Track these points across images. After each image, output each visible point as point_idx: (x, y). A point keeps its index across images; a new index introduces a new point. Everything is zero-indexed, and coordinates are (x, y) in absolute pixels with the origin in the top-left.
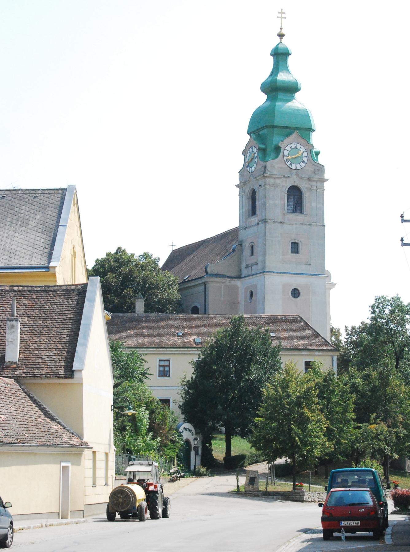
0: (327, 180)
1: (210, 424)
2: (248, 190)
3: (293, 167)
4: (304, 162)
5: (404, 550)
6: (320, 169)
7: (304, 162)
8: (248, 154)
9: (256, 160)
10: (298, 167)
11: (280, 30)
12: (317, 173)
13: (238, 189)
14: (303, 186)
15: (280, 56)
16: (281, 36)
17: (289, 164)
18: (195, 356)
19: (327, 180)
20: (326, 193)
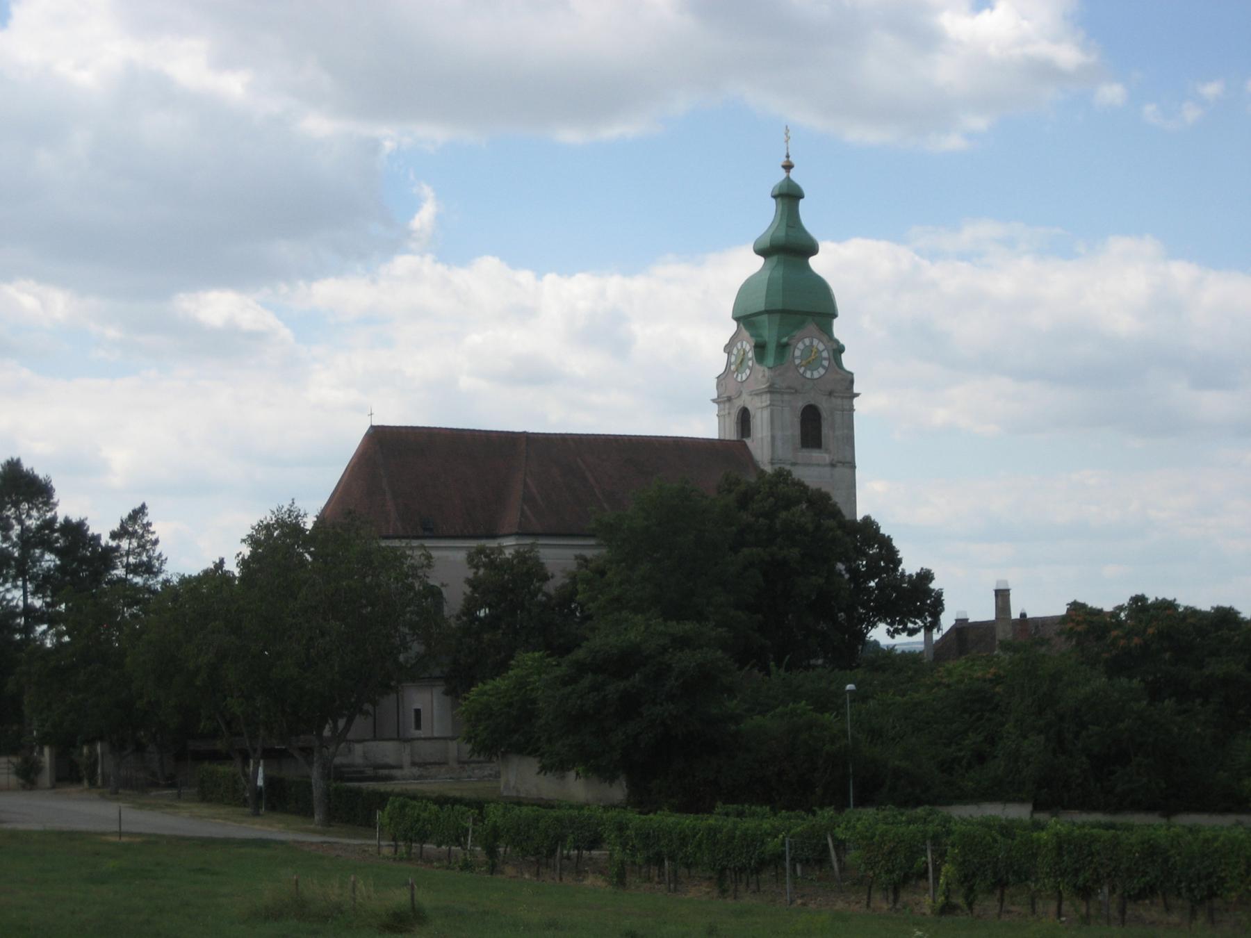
0: (857, 395)
1: (482, 571)
2: (735, 412)
3: (808, 375)
4: (824, 367)
5: (992, 872)
6: (849, 379)
7: (824, 367)
8: (735, 351)
9: (750, 363)
10: (816, 375)
11: (782, 174)
12: (844, 387)
13: (716, 406)
14: (824, 405)
15: (789, 196)
16: (788, 167)
17: (801, 370)
18: (460, 276)
19: (857, 395)
20: (855, 414)
